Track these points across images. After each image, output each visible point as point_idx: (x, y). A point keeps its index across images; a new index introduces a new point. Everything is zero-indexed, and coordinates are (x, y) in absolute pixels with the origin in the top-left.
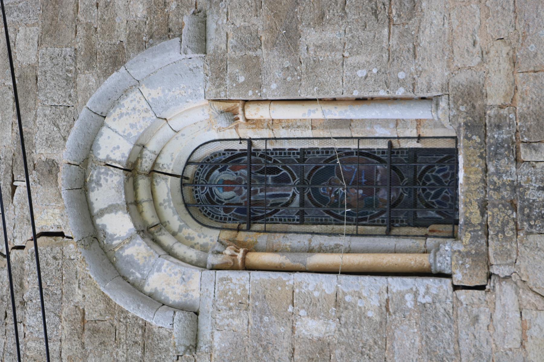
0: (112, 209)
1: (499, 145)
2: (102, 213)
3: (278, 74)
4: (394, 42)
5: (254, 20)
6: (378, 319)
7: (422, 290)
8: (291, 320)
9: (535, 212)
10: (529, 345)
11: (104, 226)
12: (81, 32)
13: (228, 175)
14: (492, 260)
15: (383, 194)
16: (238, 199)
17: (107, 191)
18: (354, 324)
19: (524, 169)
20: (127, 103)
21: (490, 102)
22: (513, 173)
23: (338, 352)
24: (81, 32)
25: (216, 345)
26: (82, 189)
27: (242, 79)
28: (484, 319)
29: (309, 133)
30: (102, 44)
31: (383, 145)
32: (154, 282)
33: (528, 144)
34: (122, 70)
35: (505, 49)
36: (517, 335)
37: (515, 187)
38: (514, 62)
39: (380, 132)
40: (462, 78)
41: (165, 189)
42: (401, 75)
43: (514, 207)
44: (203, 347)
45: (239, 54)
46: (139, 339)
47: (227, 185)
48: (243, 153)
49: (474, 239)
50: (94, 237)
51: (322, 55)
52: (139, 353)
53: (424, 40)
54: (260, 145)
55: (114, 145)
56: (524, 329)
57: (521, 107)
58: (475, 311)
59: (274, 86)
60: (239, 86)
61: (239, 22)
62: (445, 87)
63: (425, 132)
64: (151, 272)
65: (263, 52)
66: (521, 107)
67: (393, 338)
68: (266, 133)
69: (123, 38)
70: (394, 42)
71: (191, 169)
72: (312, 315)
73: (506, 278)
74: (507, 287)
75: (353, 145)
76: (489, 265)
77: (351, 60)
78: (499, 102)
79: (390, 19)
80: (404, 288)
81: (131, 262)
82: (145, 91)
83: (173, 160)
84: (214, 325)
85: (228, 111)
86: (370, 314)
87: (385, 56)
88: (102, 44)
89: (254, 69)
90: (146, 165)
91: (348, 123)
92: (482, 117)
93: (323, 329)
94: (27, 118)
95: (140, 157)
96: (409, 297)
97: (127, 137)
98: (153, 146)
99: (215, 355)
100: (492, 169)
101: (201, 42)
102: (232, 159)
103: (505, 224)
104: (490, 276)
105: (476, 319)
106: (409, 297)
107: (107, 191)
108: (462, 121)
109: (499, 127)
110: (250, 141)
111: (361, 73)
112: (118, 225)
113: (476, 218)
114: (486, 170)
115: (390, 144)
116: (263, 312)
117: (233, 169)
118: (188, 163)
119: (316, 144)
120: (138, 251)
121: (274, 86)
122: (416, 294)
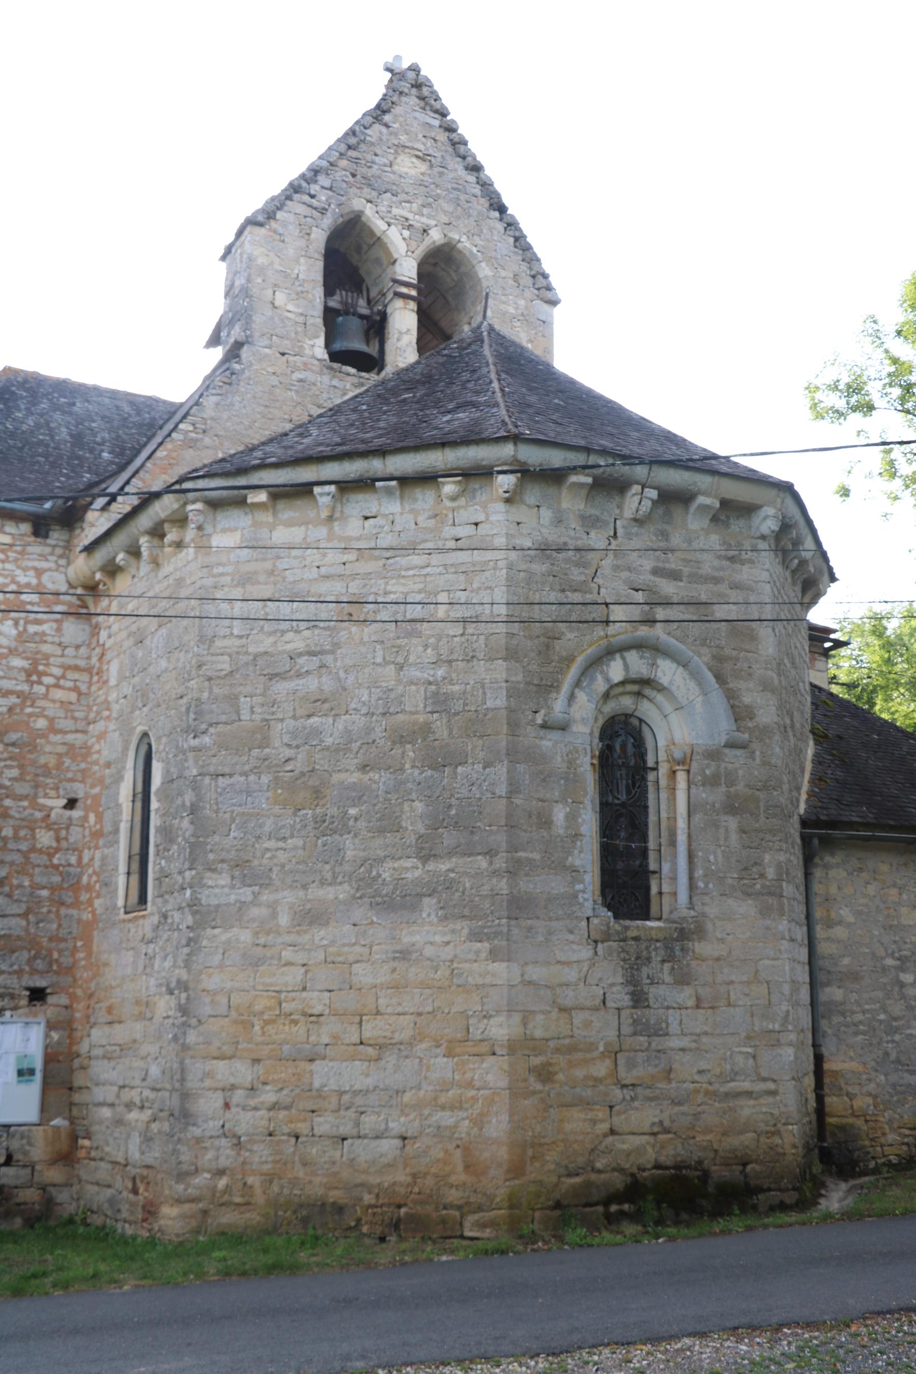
0: (626, 667)
1: (672, 950)
2: (623, 658)
3: (711, 799)
4: (730, 881)
5: (742, 783)
6: (568, 864)
7: (586, 896)
8: (563, 800)
9: (635, 973)
10: (559, 967)
11: (615, 660)
12: (734, 653)
13: (630, 750)
14: (606, 944)
15: (620, 865)
16: (616, 756)
17: (637, 663)
18: (563, 847)
19: (659, 966)
20: (692, 685)
21: (696, 944)
22: (656, 958)
23: (545, 834)
24: (734, 653)
25: (544, 742)
26: (639, 646)
27: (708, 772)
28: (571, 937)
29: (664, 815)
30: (728, 667)
31: (652, 866)
32: (581, 697)
33: (673, 968)
34: (717, 686)
35: (724, 953)
36: (563, 959)
37: (649, 959)
38: (718, 959)
39: (666, 867)
40: (709, 926)
41: (627, 703)
42: (711, 886)
43: (637, 958)
44: (542, 733)
45: (722, 771)
46: (544, 682)
47: (624, 747)
48: (645, 762)
49: (618, 933)
50: (611, 652)
51: (722, 830)
52: (535, 682)
53: (730, 901)
54: (651, 776)
55: (667, 672)
56: (568, 963)
57: (694, 963)
58: (576, 932)
59: (704, 795)
60: (703, 770)
61: (740, 772)
62: (704, 914)
63: (666, 899)
64: (587, 694)
65: (723, 788)
66: (694, 963)
67: (556, 874)
68: (663, 782)
69: (731, 685)
70: (730, 881)
71: (635, 722)
72: (567, 817)
73: (596, 953)
74: (591, 952)
75: (652, 845)
76: (602, 942)
77: (719, 852)
78: (697, 950)
79: (742, 879)
80: (587, 882)
81: (593, 679)
82: (700, 699)
83: (646, 710)
84: (557, 742)
85: (685, 758)
86: (570, 859)
87: (721, 875)
88: (728, 667)
89: (712, 781)
90: (647, 691)
91: (673, 843)
92: (689, 939)
93: (559, 824)
94: (681, 607)
95: (654, 689)
96: (581, 887)
97: (671, 683)
98: (659, 698)
99: (537, 741)
100: (658, 945)
101: (731, 745)
102: (641, 754)
103: (627, 953)
104: (596, 942)
105: (571, 932)
106: (581, 887)
107: (637, 663)
108: (685, 925)
109: (682, 950)
110: (655, 769)
111: (712, 858)
112: (616, 671)
113: (632, 933)
114: (657, 941)
115: (654, 872)
116: (567, 780)
117: (634, 754)
118: (641, 720)
119: (652, 818)
120: (600, 686)
121: (704, 795)
122: (584, 891)
